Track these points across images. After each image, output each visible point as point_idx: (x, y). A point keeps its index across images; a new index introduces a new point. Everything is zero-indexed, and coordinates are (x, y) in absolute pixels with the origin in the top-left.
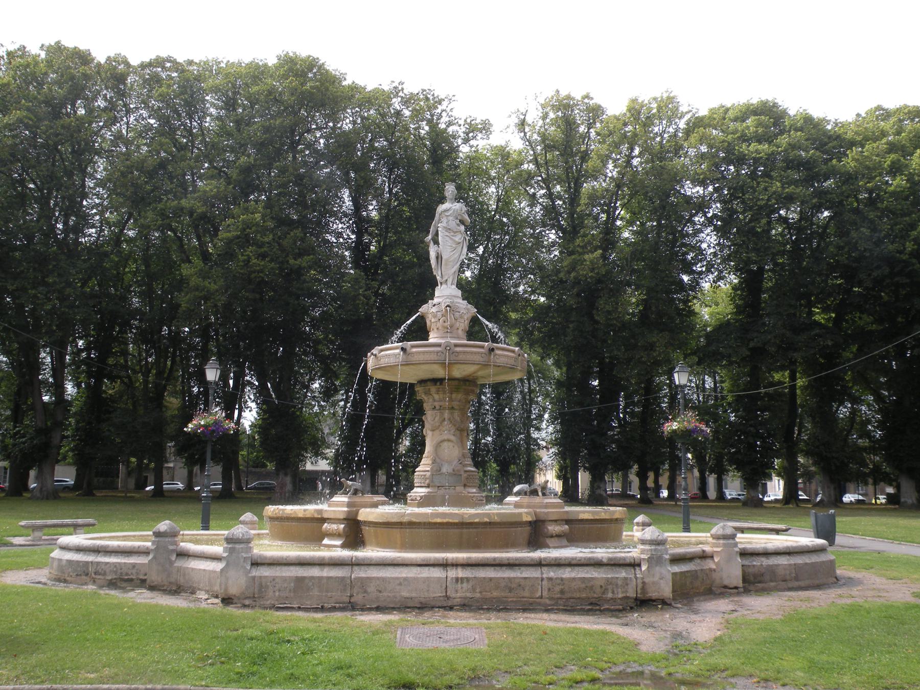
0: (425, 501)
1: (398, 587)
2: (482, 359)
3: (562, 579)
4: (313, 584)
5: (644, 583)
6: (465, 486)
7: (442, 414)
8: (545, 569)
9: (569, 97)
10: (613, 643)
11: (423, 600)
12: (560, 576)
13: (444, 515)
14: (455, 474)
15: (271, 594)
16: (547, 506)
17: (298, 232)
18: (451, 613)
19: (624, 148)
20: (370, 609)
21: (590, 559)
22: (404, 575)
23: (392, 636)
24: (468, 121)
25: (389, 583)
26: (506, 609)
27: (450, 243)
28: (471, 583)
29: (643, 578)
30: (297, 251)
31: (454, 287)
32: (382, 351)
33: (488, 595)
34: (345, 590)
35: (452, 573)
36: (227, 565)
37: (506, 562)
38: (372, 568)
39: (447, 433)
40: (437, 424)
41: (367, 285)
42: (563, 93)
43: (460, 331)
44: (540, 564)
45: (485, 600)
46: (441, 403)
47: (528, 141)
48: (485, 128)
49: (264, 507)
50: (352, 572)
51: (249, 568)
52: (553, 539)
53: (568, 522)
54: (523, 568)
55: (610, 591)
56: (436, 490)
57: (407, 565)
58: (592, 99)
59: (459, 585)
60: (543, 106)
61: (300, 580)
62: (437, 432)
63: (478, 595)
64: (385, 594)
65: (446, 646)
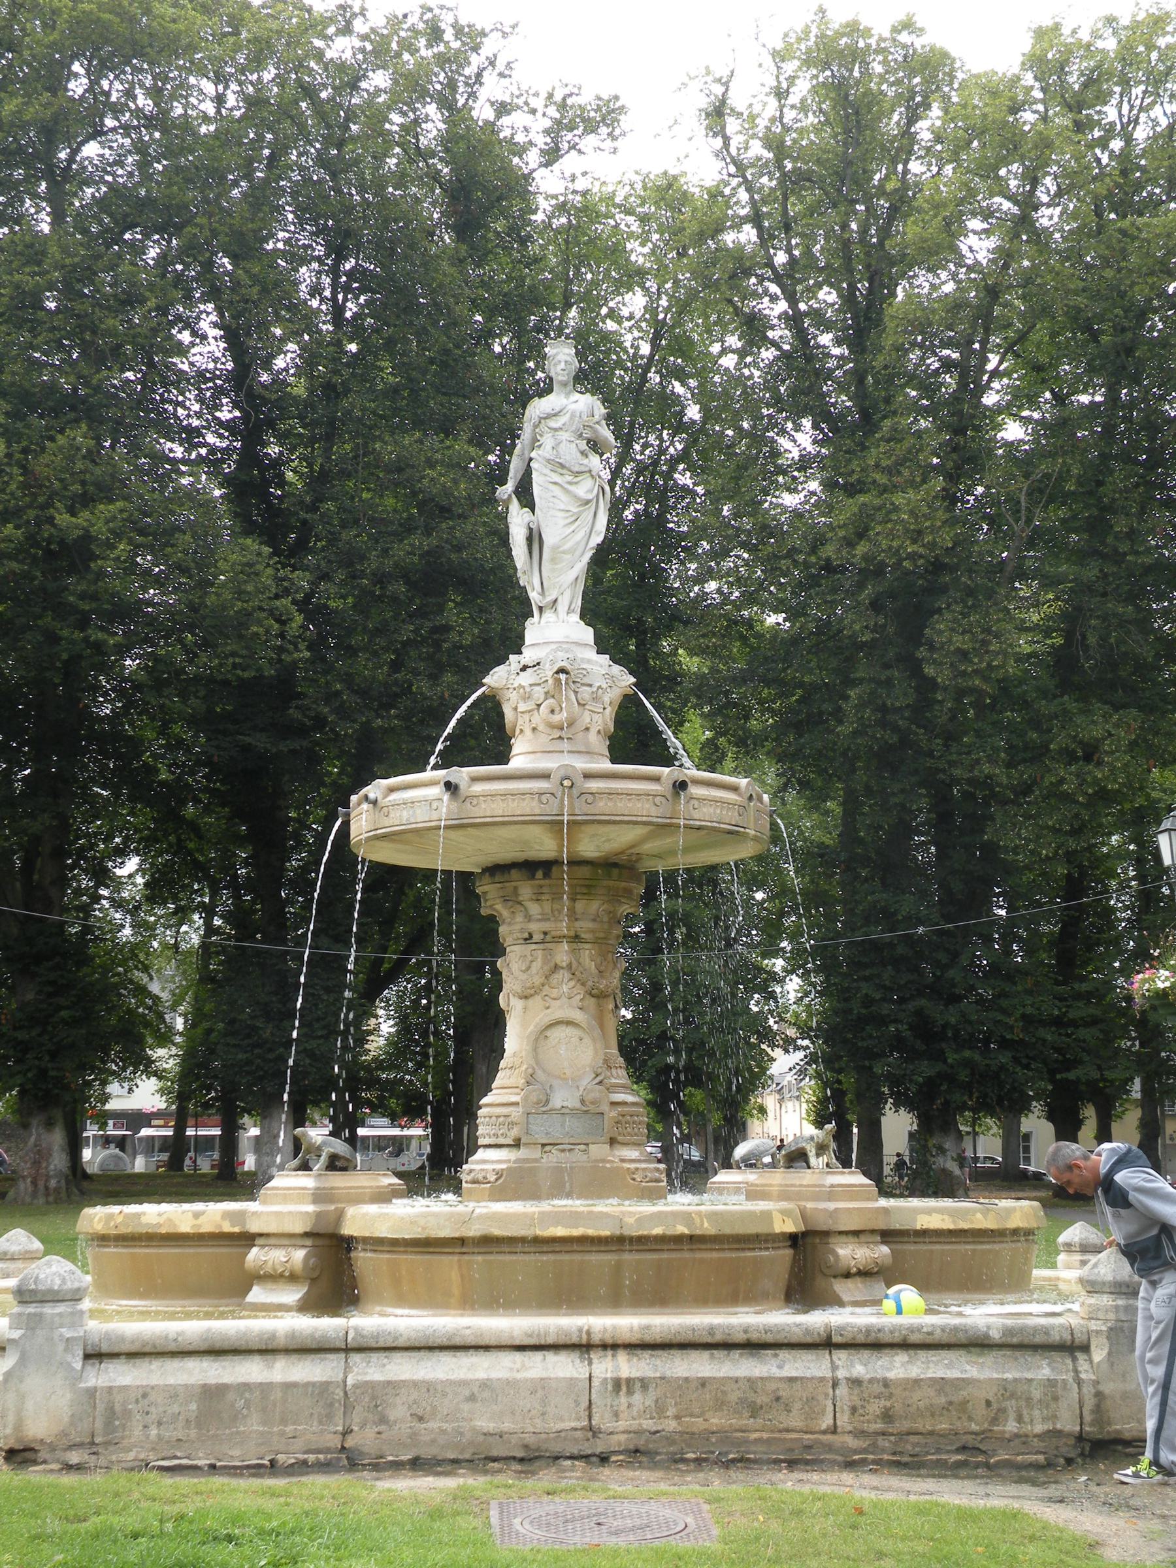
0: (510, 1185)
1: (466, 1407)
2: (654, 811)
3: (886, 1383)
4: (247, 1405)
5: (1099, 1395)
6: (613, 1142)
7: (549, 953)
8: (841, 1356)
9: (853, 28)
10: (1032, 1538)
11: (530, 1439)
12: (880, 1374)
13: (575, 1217)
14: (588, 1111)
15: (137, 1432)
16: (832, 1194)
17: (80, 436)
18: (606, 1471)
19: (1012, 174)
20: (397, 1466)
21: (955, 1329)
22: (481, 1375)
23: (477, 1523)
24: (558, 97)
25: (445, 1395)
26: (743, 1462)
27: (564, 502)
28: (652, 1395)
29: (1096, 1383)
30: (76, 488)
31: (575, 617)
32: (392, 790)
33: (698, 1424)
34: (330, 1417)
35: (605, 1367)
36: (23, 1361)
37: (740, 1337)
38: (397, 1357)
39: (567, 1000)
40: (538, 980)
41: (279, 580)
42: (838, 18)
43: (593, 737)
44: (827, 1343)
45: (691, 1437)
46: (546, 926)
47: (734, 162)
48: (605, 117)
49: (80, 1207)
50: (347, 1370)
51: (78, 1364)
52: (850, 1283)
53: (887, 1236)
54: (783, 1354)
55: (1012, 1415)
56: (536, 1153)
57: (487, 1348)
58: (921, 31)
59: (623, 1399)
60: (780, 56)
61: (212, 1394)
62: (536, 1002)
63: (671, 1425)
64: (433, 1425)
65: (621, 1542)
